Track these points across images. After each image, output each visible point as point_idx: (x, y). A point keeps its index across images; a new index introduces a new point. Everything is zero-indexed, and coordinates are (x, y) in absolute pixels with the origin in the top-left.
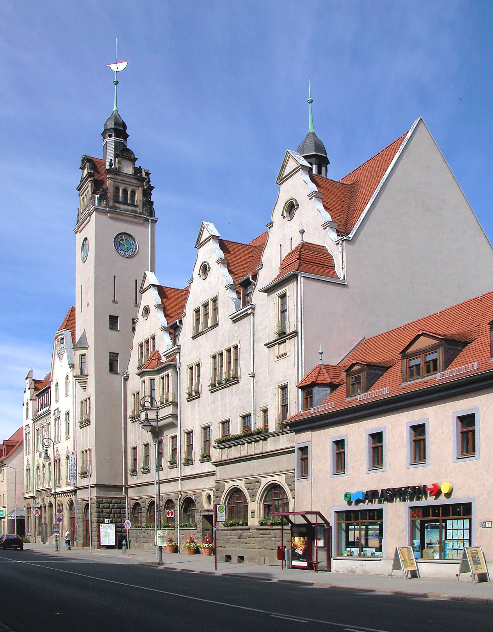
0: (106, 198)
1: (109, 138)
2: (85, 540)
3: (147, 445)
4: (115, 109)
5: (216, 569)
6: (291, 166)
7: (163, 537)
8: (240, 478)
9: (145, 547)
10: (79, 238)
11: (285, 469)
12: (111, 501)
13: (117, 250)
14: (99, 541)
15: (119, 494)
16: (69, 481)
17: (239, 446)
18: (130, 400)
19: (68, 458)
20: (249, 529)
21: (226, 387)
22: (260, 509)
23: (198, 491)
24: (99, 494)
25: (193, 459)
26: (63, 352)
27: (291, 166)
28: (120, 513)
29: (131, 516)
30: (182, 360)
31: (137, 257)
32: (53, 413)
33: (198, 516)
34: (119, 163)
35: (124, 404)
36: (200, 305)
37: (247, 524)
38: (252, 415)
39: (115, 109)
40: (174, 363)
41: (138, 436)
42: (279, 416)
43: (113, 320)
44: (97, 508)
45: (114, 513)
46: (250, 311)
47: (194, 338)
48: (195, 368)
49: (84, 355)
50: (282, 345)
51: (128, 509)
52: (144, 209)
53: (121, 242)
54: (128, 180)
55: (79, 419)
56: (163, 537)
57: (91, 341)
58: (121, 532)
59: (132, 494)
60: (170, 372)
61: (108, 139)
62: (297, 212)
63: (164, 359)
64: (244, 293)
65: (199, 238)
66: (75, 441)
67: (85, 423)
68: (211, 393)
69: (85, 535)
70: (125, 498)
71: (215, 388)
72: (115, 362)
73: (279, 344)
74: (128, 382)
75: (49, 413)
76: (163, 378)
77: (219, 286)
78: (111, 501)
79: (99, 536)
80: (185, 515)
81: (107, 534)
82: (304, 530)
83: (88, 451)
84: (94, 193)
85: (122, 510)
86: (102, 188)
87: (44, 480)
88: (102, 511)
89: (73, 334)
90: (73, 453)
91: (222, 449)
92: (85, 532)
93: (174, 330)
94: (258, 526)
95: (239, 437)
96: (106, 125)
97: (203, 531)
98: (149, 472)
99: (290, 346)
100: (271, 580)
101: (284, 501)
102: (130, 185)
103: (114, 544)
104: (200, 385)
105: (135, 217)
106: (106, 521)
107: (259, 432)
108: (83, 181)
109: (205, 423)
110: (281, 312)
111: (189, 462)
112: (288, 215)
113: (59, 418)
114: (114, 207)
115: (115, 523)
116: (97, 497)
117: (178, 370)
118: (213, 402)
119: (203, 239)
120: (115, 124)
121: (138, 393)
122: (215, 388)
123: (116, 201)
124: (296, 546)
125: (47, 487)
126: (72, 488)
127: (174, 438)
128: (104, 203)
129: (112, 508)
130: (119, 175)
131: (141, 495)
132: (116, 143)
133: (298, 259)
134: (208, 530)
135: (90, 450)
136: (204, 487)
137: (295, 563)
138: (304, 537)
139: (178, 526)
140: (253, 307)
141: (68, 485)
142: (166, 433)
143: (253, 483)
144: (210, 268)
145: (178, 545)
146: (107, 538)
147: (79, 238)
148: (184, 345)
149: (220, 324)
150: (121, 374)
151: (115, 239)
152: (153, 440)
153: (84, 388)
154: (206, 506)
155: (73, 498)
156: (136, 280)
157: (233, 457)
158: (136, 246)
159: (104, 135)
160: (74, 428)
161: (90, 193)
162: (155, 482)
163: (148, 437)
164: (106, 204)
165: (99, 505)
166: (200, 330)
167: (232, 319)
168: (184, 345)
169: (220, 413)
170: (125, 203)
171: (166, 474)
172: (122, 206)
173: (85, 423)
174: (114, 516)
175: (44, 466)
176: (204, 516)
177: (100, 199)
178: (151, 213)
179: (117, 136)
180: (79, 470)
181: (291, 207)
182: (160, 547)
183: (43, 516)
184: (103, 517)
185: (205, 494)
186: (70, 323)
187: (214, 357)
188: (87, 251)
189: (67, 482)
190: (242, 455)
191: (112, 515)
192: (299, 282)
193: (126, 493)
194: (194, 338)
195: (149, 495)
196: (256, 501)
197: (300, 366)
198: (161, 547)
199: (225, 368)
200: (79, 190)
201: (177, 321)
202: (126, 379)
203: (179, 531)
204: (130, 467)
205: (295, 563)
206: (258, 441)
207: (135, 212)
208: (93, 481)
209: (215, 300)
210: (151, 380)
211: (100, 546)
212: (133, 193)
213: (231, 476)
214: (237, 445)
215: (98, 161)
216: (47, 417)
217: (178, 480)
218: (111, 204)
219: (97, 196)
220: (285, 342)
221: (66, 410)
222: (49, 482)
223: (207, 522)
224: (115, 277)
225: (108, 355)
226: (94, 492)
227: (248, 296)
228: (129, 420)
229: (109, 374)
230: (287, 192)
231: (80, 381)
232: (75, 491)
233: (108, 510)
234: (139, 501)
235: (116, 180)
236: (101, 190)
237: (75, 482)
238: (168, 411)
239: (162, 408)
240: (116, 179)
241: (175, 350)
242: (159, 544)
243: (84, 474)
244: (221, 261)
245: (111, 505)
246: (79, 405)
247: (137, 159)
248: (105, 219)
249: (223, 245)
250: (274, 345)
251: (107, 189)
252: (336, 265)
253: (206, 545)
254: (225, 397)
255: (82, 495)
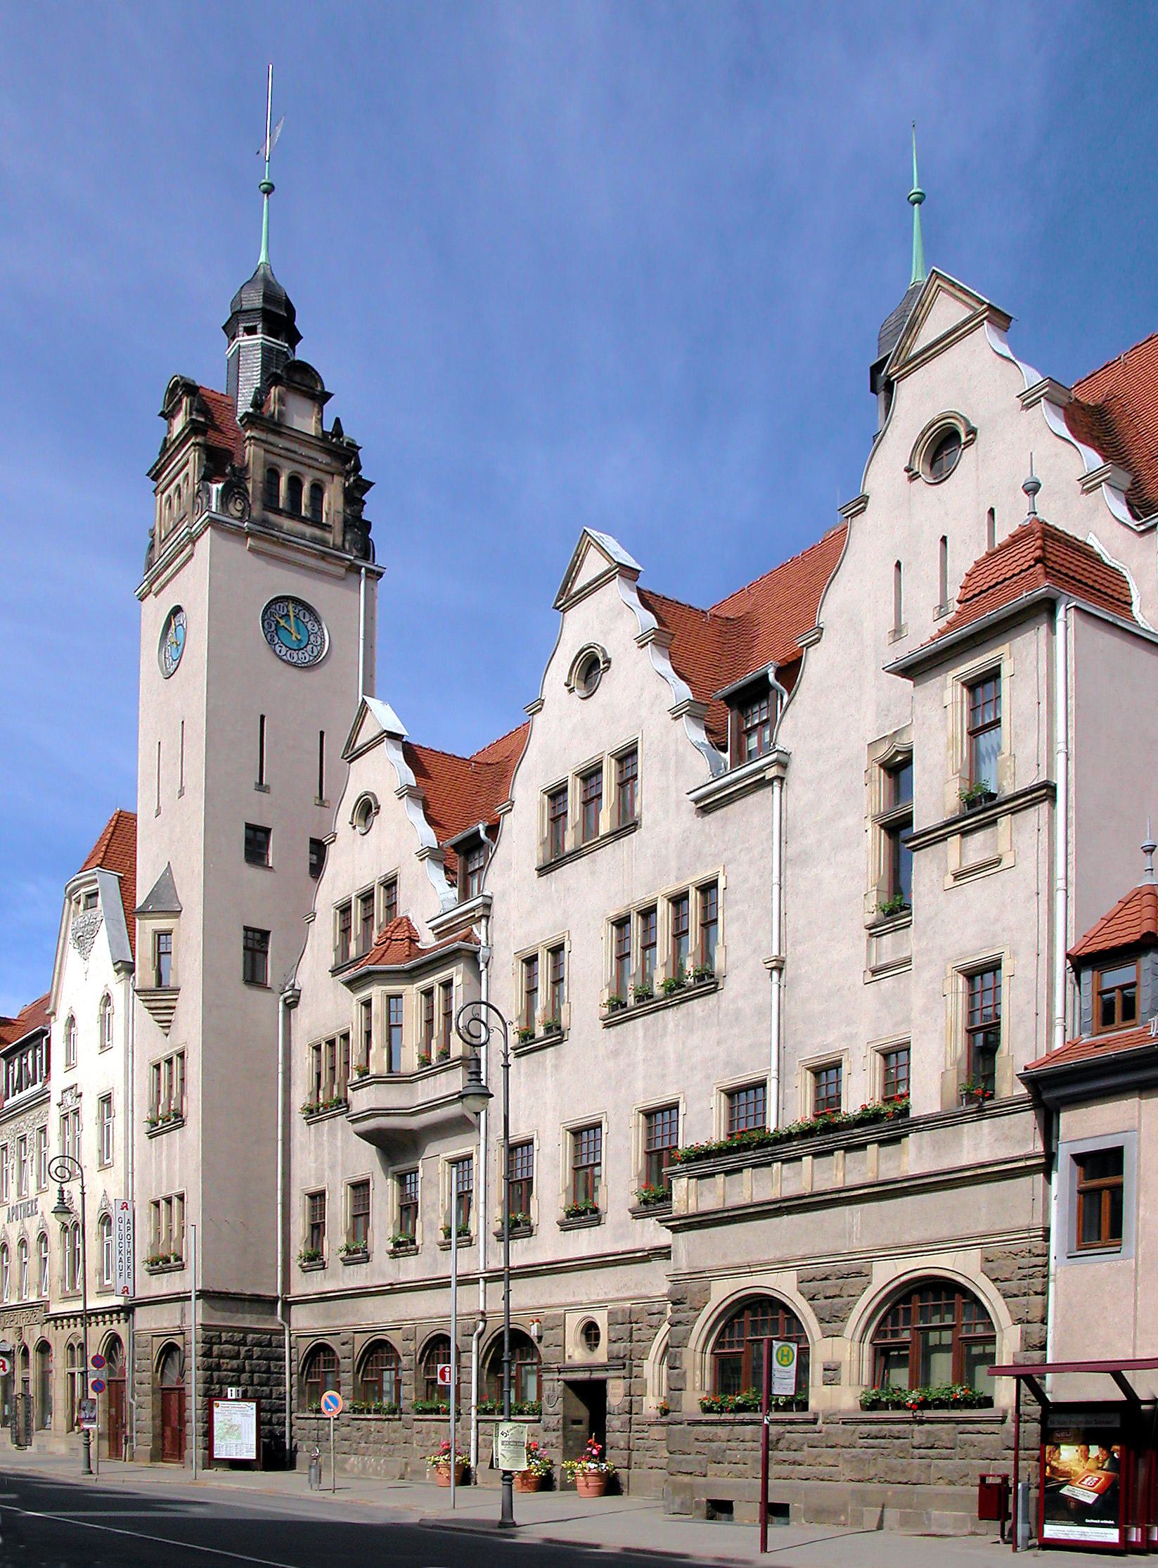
0: (244, 495)
1: (247, 337)
2: (160, 1443)
3: (360, 1188)
4: (262, 259)
5: (764, 1548)
6: (593, 566)
7: (517, 1443)
8: (783, 1265)
9: (348, 1467)
10: (154, 612)
11: (981, 1229)
12: (244, 1338)
13: (271, 642)
14: (210, 1447)
15: (265, 1321)
16: (107, 1282)
17: (777, 1165)
18: (303, 1062)
19: (106, 1220)
20: (815, 1422)
21: (666, 1007)
22: (860, 1360)
23: (547, 1312)
24: (211, 1318)
25: (534, 1221)
26: (94, 933)
27: (593, 566)
28: (268, 1371)
29: (299, 1381)
30: (496, 937)
31: (324, 669)
32: (56, 1097)
33: (551, 1383)
34: (281, 400)
35: (284, 1073)
36: (570, 774)
37: (804, 1406)
38: (772, 1087)
39: (262, 259)
40: (472, 946)
41: (330, 1157)
42: (957, 1062)
43: (256, 843)
44: (203, 1355)
45: (252, 1372)
46: (771, 773)
47: (544, 870)
48: (544, 965)
49: (168, 933)
50: (979, 836)
51: (291, 1361)
52: (348, 537)
53: (282, 622)
54: (304, 451)
55: (142, 1112)
56: (517, 1443)
57: (191, 894)
58: (270, 1422)
59: (304, 1320)
60: (457, 973)
61: (244, 340)
62: (376, 821)
63: (427, 940)
64: (465, 867)
65: (570, 578)
66: (130, 1173)
67: (166, 1121)
68: (607, 1026)
69: (159, 1430)
70: (281, 1332)
71: (618, 1012)
72: (259, 956)
73: (965, 833)
74: (297, 1012)
75: (43, 1099)
76: (428, 993)
77: (644, 712)
78: (244, 1338)
79: (209, 1434)
80: (492, 1379)
81: (232, 1429)
82: (1115, 1422)
83: (175, 1201)
84: (207, 477)
85: (272, 1363)
86: (233, 466)
87: (21, 1281)
88: (218, 1365)
89: (127, 886)
90: (125, 1206)
91: (700, 1177)
92: (158, 1422)
93: (465, 854)
94: (855, 1411)
95: (807, 1133)
96: (238, 299)
97: (564, 1424)
98: (367, 1259)
99: (1016, 836)
100: (512, 1536)
101: (960, 1331)
102: (310, 466)
103: (253, 1456)
104: (564, 1007)
105: (324, 556)
106: (232, 1392)
107: (869, 1118)
108: (168, 450)
109: (581, 1116)
110: (970, 733)
111: (357, 1254)
112: (928, 470)
113: (76, 1112)
114: (264, 522)
115: (257, 1399)
116: (205, 1327)
117: (482, 966)
118: (615, 1054)
119: (580, 583)
120: (266, 298)
121: (346, 1037)
122: (618, 1012)
123: (270, 502)
124: (1066, 1474)
125: (33, 1299)
126: (120, 1301)
127: (462, 1162)
128: (236, 508)
129: (245, 1358)
130: (279, 434)
131: (339, 1322)
132: (266, 350)
133: (1038, 560)
134: (579, 1422)
135: (181, 1198)
136: (570, 1299)
137: (1052, 1531)
138: (1105, 1445)
139: (473, 1411)
140: (783, 758)
141: (104, 1291)
142: (431, 1149)
143: (832, 1282)
144: (608, 661)
145: (472, 1464)
146: (232, 1441)
147: (154, 612)
148: (503, 894)
149: (646, 821)
150: (277, 989)
151: (265, 612)
152: (385, 1170)
153: (166, 1025)
154: (576, 1353)
155: (121, 1329)
156: (322, 733)
157: (747, 1201)
158: (323, 638)
159: (230, 330)
160: (126, 1138)
161: (194, 478)
162: (453, 1280)
163: (366, 1160)
164: (243, 511)
165: (211, 1349)
166: (569, 846)
167: (696, 801)
168: (503, 894)
169: (640, 1085)
170: (294, 513)
171: (383, 1268)
172: (288, 524)
173: (166, 1121)
174: (251, 1378)
175: (23, 1243)
176: (569, 1384)
177: (225, 496)
178: (366, 551)
179: (269, 331)
180: (143, 1252)
181: (591, 667)
182: (506, 1473)
183: (18, 1376)
184: (221, 1382)
185: (574, 1322)
186: (118, 845)
187: (621, 923)
188: (180, 647)
189: (101, 1284)
190: (786, 1194)
191: (245, 1377)
192: (1060, 626)
193: (286, 1316)
194: (544, 870)
195: (365, 1323)
196: (848, 1332)
197: (1060, 896)
198: (509, 1473)
199: (663, 951)
200: (155, 478)
201: (481, 827)
202: (291, 1005)
203: (474, 1424)
204: (299, 1246)
205: (1052, 1531)
206: (862, 1147)
207: (323, 542)
208: (188, 1281)
209: (627, 756)
210: (390, 997)
211: (211, 1461)
212: (317, 490)
213: (737, 1260)
214: (769, 1164)
215: (215, 396)
216: (35, 1112)
217: (476, 1281)
218: (254, 514)
219: (216, 487)
220: (994, 822)
221: (103, 1089)
222: (39, 1286)
223: (575, 1401)
224: (262, 718)
225: (241, 933)
226: (196, 1313)
227: (749, 736)
228: (298, 1118)
229: (244, 988)
230: (919, 402)
231: (153, 1004)
232: (127, 1311)
233: (235, 1363)
234: (327, 1340)
235: (270, 448)
236: (228, 470)
237: (130, 1284)
238: (455, 1081)
239: (426, 1077)
240: (271, 444)
241: (473, 909)
242: (504, 1465)
243: (162, 1264)
244: (409, 792)
245: (243, 1350)
246: (143, 1077)
247: (330, 395)
248: (238, 551)
249: (412, 755)
250: (943, 838)
251: (245, 469)
252: (1134, 599)
253: (592, 1466)
254: (664, 1035)
255: (145, 1319)
